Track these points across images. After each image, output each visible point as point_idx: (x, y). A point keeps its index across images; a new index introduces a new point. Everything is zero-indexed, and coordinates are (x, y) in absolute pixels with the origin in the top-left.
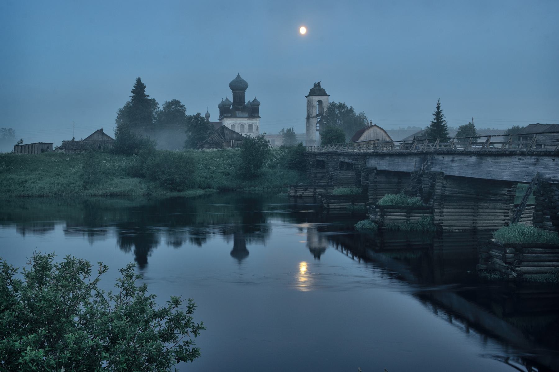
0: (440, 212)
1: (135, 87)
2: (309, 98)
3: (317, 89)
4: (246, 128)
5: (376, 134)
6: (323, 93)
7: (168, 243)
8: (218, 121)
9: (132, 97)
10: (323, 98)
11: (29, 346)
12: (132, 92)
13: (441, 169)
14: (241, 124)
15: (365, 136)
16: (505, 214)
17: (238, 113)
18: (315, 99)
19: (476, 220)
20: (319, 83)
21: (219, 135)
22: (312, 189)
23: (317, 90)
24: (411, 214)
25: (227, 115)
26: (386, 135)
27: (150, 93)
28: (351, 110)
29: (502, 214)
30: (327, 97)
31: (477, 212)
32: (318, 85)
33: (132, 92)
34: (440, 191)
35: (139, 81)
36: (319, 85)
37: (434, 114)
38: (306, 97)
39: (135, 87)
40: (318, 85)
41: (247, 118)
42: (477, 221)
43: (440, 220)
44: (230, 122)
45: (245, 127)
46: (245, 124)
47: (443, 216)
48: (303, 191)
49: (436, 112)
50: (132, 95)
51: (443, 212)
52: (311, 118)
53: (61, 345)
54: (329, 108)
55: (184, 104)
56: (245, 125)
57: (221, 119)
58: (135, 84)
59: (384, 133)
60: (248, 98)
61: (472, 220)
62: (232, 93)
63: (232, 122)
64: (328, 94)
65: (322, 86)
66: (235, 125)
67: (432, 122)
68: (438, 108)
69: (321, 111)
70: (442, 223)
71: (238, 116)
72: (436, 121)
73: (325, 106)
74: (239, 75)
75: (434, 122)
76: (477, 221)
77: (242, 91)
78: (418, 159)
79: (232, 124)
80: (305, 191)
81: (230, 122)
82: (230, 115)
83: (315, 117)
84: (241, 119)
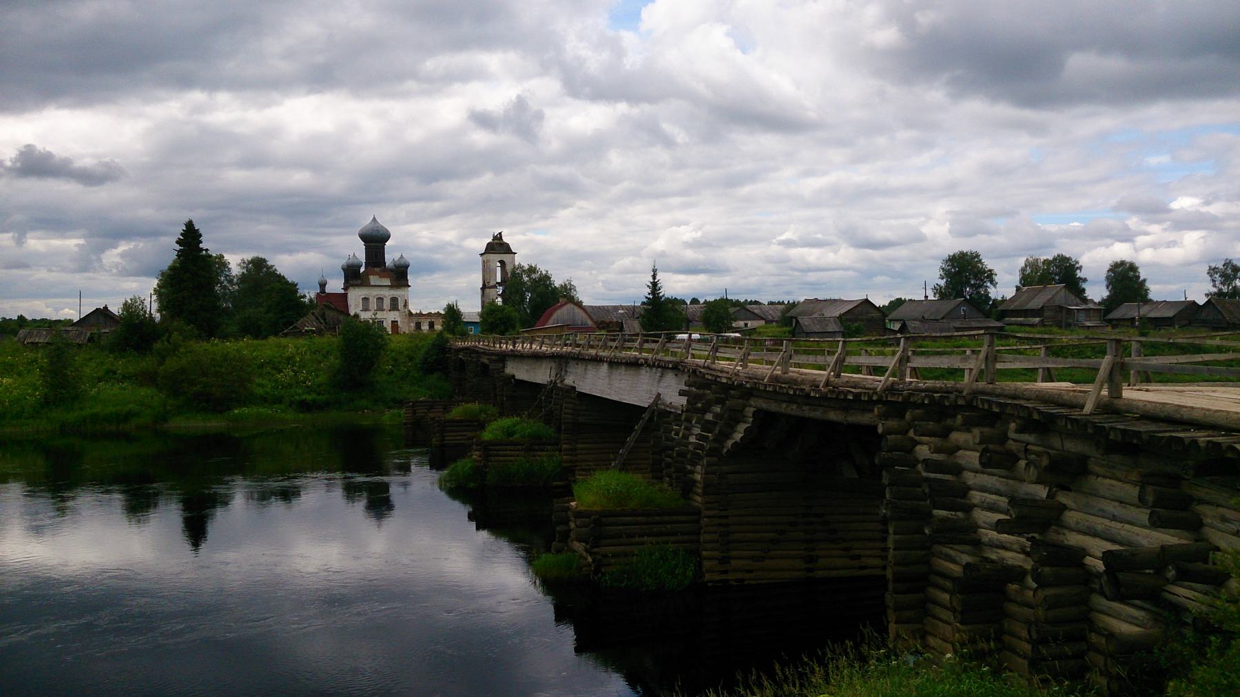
0: (571, 450)
1: (182, 234)
2: (485, 255)
3: (496, 243)
4: (373, 304)
5: (571, 314)
6: (506, 249)
7: (250, 497)
8: (343, 292)
9: (178, 251)
10: (506, 257)
12: (177, 242)
13: (574, 382)
14: (379, 296)
17: (374, 280)
18: (495, 258)
20: (500, 234)
21: (317, 318)
22: (440, 407)
25: (355, 282)
26: (587, 317)
27: (209, 244)
28: (547, 277)
30: (513, 255)
32: (498, 238)
33: (177, 242)
34: (570, 416)
35: (190, 225)
36: (501, 238)
38: (481, 255)
39: (182, 234)
40: (498, 238)
41: (389, 288)
43: (571, 461)
44: (360, 294)
45: (385, 301)
46: (385, 297)
47: (576, 455)
48: (426, 411)
50: (178, 247)
51: (576, 449)
52: (488, 288)
54: (513, 273)
55: (272, 264)
56: (385, 299)
57: (345, 288)
59: (584, 314)
60: (391, 256)
63: (364, 293)
65: (505, 239)
66: (383, 299)
67: (646, 298)
68: (654, 277)
70: (576, 466)
71: (372, 283)
72: (651, 297)
73: (509, 268)
74: (374, 218)
75: (649, 299)
78: (553, 365)
79: (363, 297)
80: (429, 410)
81: (360, 294)
82: (359, 282)
83: (495, 287)
84: (379, 289)
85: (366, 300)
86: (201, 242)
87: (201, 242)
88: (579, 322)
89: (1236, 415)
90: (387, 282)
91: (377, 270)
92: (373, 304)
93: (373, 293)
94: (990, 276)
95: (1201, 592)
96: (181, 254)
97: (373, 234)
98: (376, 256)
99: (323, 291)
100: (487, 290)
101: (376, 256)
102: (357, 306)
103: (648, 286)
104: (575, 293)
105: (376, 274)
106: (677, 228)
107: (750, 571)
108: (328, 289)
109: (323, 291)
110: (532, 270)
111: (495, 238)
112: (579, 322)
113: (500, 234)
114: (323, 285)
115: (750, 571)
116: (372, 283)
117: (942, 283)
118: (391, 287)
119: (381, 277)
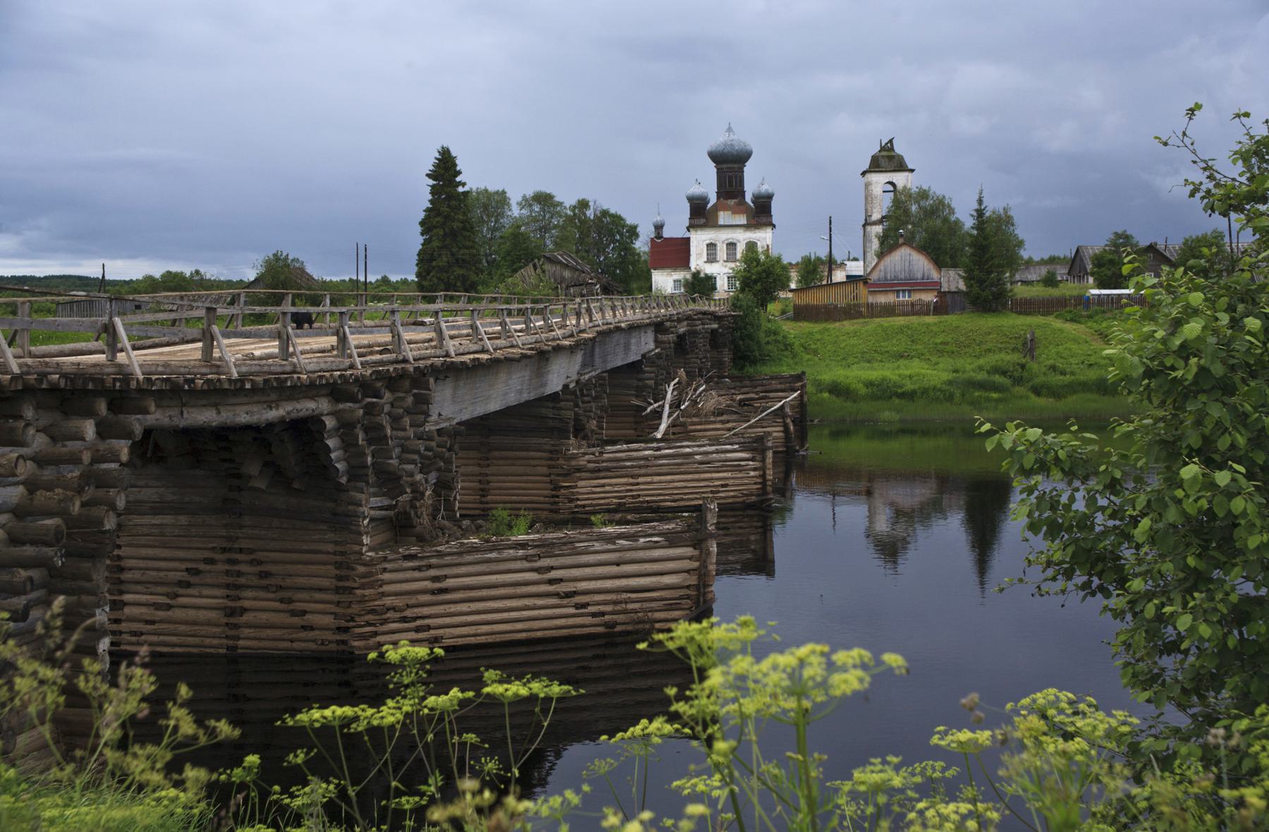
4: (722, 252)
5: (907, 264)
6: (900, 166)
10: (900, 179)
11: (1244, 772)
15: (882, 268)
16: (550, 462)
17: (724, 217)
18: (879, 181)
19: (487, 475)
20: (891, 141)
23: (887, 160)
24: (109, 441)
27: (472, 178)
29: (544, 462)
30: (906, 174)
31: (488, 459)
32: (888, 148)
36: (892, 149)
37: (972, 216)
38: (864, 174)
40: (888, 148)
42: (489, 478)
49: (977, 211)
50: (431, 182)
53: (710, 731)
58: (436, 159)
60: (753, 181)
61: (477, 475)
62: (715, 170)
64: (910, 167)
65: (899, 149)
69: (659, 227)
71: (721, 222)
76: (489, 478)
77: (736, 166)
79: (708, 242)
82: (702, 221)
85: (712, 246)
86: (459, 173)
87: (459, 173)
88: (919, 275)
89: (837, 402)
90: (742, 220)
91: (732, 202)
92: (722, 252)
93: (721, 237)
94: (633, 232)
95: (223, 598)
96: (435, 191)
97: (726, 151)
98: (730, 182)
99: (659, 236)
100: (869, 228)
101: (730, 182)
102: (699, 255)
103: (972, 216)
104: (1012, 228)
105: (725, 209)
106: (175, 268)
107: (153, 622)
108: (667, 233)
109: (659, 236)
110: (923, 194)
111: (883, 149)
112: (919, 275)
113: (891, 141)
114: (659, 227)
115: (148, 622)
116: (721, 222)
117: (702, 275)
118: (747, 227)
119: (734, 212)
